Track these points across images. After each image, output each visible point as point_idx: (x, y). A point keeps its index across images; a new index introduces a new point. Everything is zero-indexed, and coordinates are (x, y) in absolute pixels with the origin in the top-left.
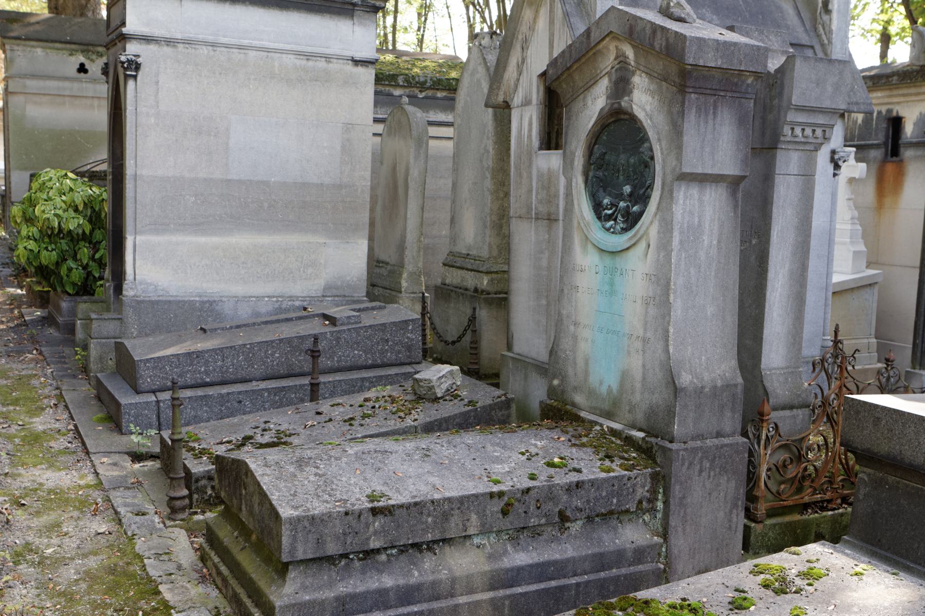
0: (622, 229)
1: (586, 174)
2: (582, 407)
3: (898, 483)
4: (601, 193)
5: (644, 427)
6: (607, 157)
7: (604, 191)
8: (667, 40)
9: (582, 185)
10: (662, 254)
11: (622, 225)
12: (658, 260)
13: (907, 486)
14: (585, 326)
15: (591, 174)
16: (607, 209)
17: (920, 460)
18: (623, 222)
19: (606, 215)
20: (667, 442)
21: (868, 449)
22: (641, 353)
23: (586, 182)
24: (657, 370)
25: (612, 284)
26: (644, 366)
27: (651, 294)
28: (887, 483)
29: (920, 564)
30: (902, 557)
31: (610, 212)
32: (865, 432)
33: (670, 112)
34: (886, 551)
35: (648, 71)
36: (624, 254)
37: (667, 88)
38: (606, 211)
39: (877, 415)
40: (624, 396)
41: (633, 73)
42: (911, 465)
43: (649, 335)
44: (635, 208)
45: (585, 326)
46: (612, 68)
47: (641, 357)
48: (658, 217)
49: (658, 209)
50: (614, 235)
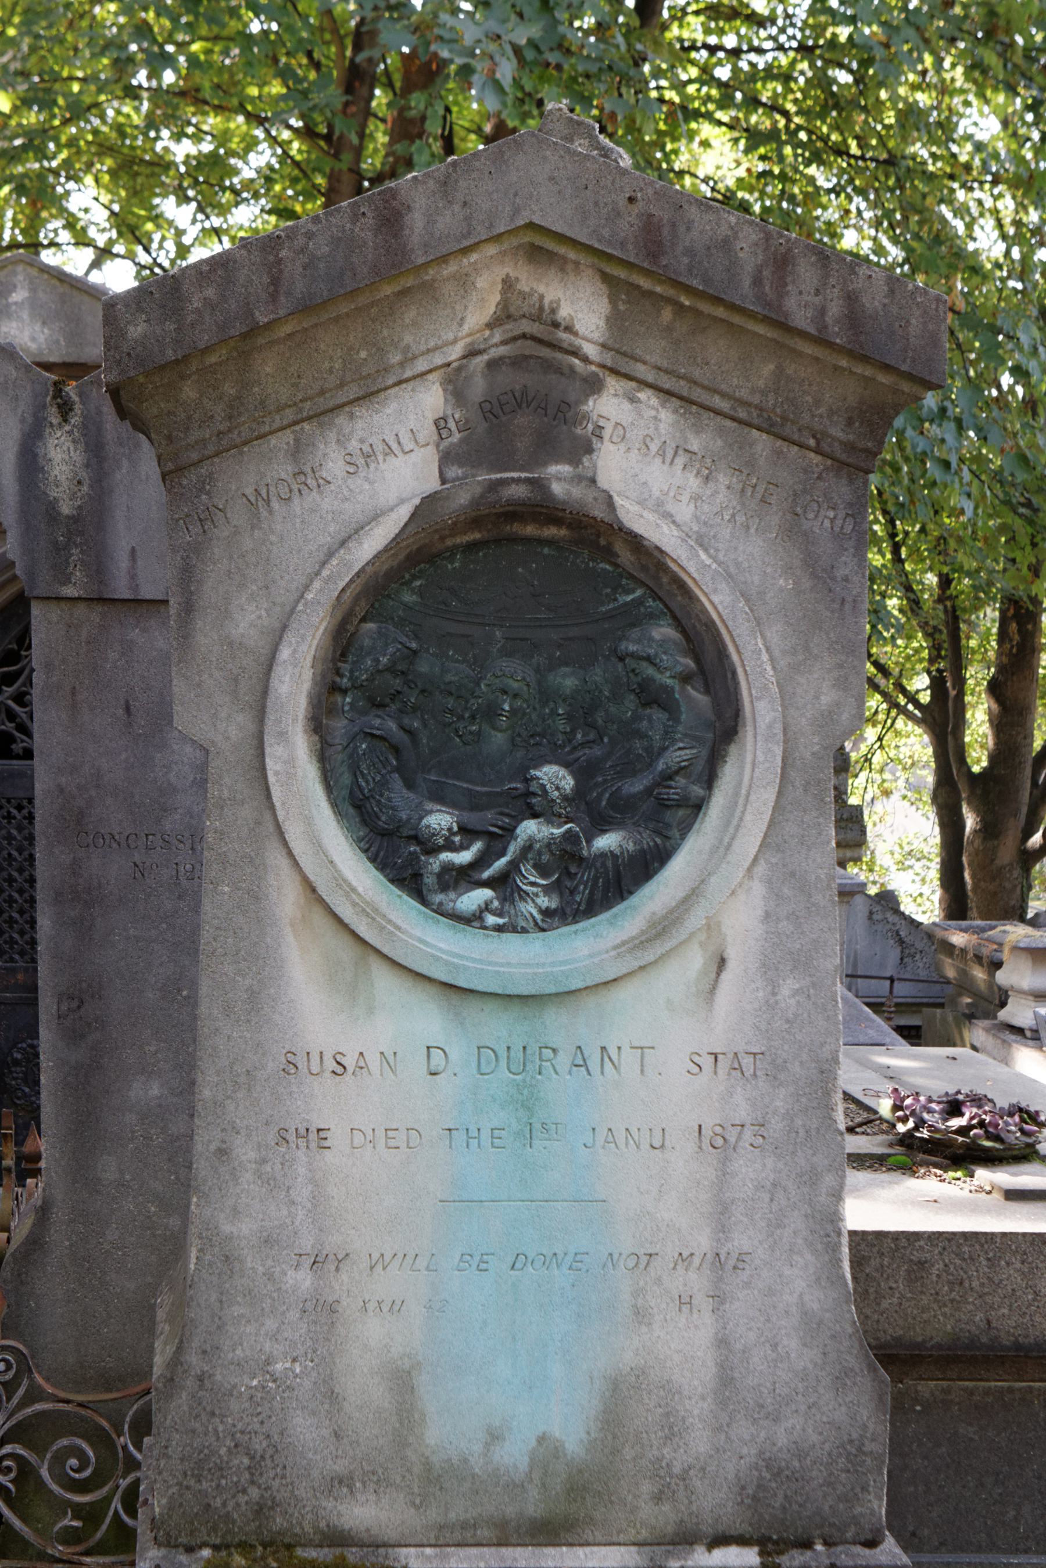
0: (546, 913)
1: (317, 725)
2: (392, 1535)
3: (947, 1391)
4: (400, 797)
5: (742, 1528)
6: (423, 667)
7: (410, 785)
8: (851, 298)
9: (309, 772)
10: (788, 986)
11: (544, 901)
12: (771, 1005)
13: (971, 1393)
14: (377, 1263)
15: (339, 726)
16: (450, 847)
17: (1045, 1327)
18: (547, 890)
19: (448, 868)
20: (858, 1549)
21: (898, 1340)
22: (706, 1305)
23: (323, 757)
24: (792, 1344)
25: (526, 1101)
26: (722, 1342)
27: (742, 1112)
28: (916, 1401)
29: (1026, 1551)
30: (979, 1549)
31: (464, 857)
32: (885, 1304)
33: (794, 530)
34: (936, 1550)
35: (667, 383)
36: (590, 1002)
37: (779, 453)
38: (446, 856)
39: (916, 1256)
40: (628, 1453)
41: (594, 386)
42: (1018, 1346)
43: (741, 1240)
44: (607, 842)
45: (377, 1263)
46: (472, 353)
47: (708, 1318)
48: (761, 869)
49: (764, 845)
50: (510, 939)
